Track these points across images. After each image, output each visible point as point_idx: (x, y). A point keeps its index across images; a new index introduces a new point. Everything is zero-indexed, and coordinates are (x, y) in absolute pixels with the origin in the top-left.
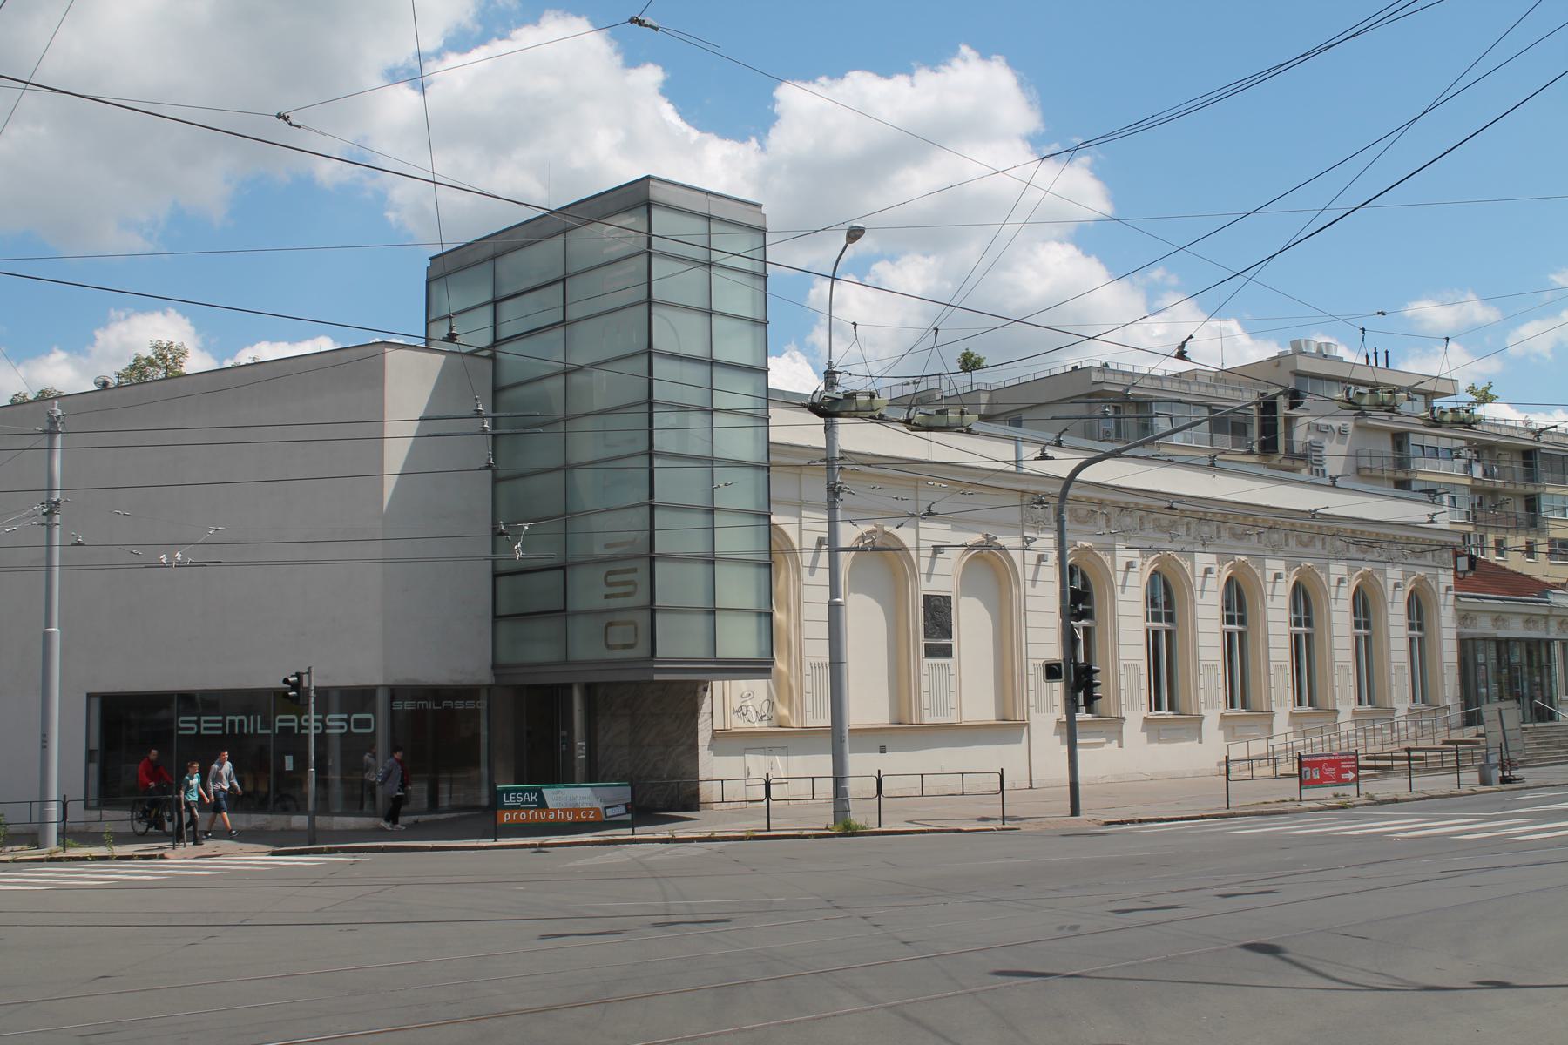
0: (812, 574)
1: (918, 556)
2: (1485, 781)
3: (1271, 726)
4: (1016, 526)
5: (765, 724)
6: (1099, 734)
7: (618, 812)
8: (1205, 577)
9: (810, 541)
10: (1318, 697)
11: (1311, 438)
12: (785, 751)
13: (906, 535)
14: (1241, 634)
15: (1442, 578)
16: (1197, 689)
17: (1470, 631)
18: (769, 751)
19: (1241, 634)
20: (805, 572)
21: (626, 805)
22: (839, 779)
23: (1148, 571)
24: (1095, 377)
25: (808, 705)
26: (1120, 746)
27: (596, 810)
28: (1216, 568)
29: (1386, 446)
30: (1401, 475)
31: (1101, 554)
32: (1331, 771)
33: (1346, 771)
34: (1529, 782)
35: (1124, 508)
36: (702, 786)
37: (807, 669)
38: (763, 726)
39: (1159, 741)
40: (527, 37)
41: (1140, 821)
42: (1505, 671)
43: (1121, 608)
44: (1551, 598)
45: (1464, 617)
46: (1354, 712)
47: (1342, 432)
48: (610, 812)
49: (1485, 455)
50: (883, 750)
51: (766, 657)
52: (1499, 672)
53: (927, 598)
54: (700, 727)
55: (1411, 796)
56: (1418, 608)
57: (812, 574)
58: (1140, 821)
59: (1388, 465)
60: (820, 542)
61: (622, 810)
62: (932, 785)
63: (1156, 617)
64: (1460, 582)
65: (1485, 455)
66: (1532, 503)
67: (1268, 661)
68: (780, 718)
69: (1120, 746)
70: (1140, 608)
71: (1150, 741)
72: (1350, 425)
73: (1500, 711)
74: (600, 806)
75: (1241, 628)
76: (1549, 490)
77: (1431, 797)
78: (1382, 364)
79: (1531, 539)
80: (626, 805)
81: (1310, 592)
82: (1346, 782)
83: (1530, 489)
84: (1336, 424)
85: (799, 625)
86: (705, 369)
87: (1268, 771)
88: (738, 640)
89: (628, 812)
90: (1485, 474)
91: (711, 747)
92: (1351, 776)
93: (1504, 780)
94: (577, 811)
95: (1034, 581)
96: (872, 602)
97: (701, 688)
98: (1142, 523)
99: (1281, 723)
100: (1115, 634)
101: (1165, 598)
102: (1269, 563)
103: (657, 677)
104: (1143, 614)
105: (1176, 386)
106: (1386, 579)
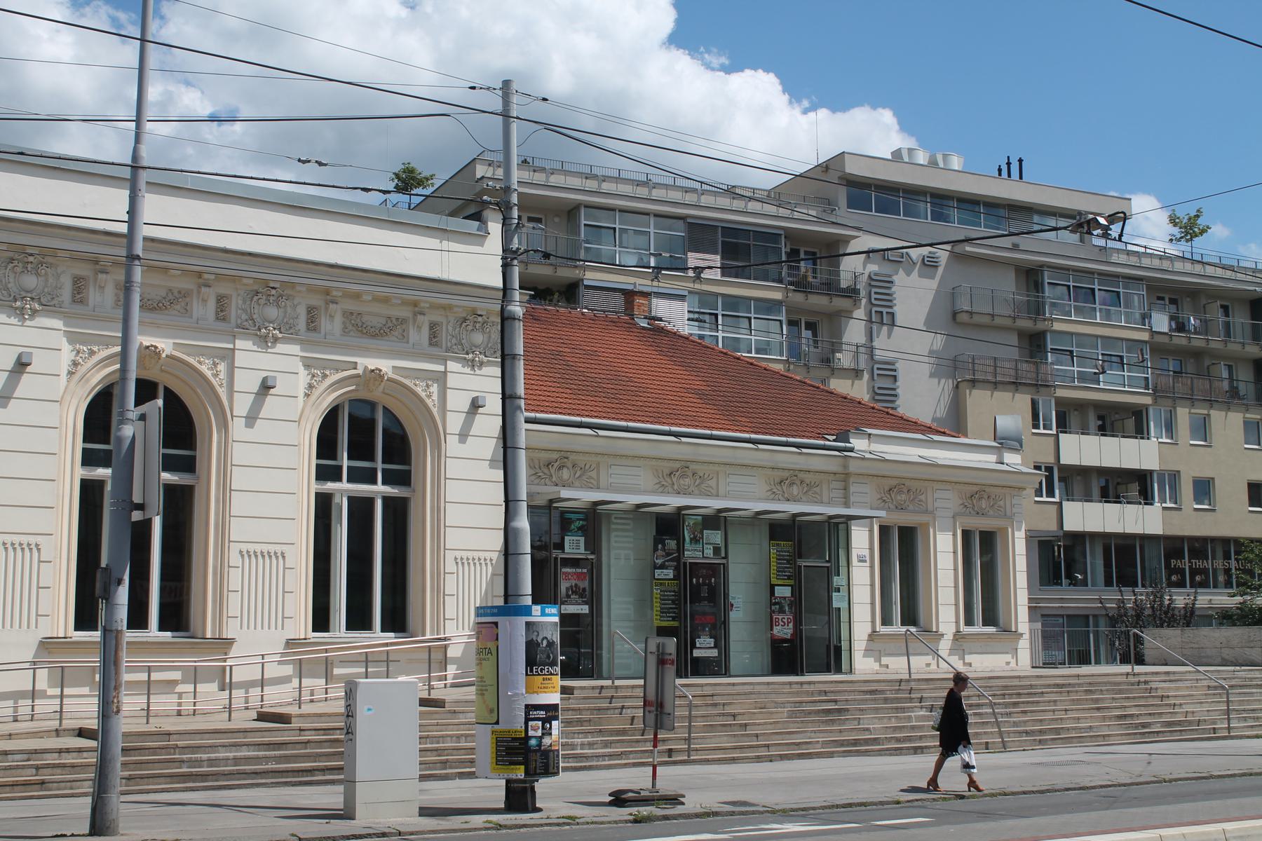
72: (943, 254)
95: (463, 436)
105: (771, 209)
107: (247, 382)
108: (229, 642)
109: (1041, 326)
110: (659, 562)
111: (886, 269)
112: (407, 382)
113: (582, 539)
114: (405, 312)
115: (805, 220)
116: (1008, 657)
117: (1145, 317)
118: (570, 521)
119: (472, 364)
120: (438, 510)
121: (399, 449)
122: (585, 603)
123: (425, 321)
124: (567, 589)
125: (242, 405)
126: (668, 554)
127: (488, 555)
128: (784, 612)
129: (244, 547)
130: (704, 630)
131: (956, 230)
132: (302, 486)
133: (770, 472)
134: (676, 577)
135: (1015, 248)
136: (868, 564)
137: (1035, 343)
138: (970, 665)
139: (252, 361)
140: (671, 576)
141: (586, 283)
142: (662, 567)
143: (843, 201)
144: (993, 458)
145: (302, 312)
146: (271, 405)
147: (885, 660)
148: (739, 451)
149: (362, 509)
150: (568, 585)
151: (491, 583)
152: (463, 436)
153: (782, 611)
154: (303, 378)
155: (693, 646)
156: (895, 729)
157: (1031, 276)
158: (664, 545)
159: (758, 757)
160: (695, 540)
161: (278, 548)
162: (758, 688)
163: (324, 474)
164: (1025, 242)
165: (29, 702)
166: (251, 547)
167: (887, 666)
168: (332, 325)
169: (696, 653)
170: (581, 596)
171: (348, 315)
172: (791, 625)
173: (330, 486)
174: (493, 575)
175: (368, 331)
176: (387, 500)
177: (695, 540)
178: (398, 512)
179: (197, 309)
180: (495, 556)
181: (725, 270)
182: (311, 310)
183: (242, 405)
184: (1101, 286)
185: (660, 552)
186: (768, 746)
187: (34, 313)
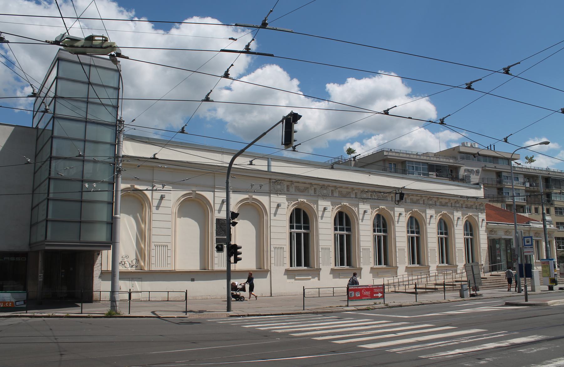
0: (322, 219)
1: (359, 214)
2: (462, 296)
3: (397, 272)
4: (149, 182)
5: (134, 268)
6: (308, 275)
7: (20, 304)
8: (430, 218)
9: (218, 201)
10: (475, 260)
11: (466, 174)
12: (140, 279)
13: (264, 199)
14: (417, 238)
15: (480, 216)
16: (359, 257)
17: (494, 236)
18: (132, 279)
19: (417, 238)
20: (154, 209)
21: (24, 301)
22: (113, 292)
23: (438, 218)
24: (385, 154)
25: (273, 261)
26: (319, 280)
27: (12, 302)
28: (461, 217)
29: (494, 176)
30: (499, 186)
31: (450, 215)
32: (368, 293)
33: (377, 293)
34: (485, 296)
35: (323, 187)
36: (94, 293)
37: (153, 247)
38: (133, 269)
39: (339, 278)
40: (259, 71)
41: (249, 315)
42: (509, 251)
43: (456, 232)
44: (531, 224)
45: (490, 231)
46: (438, 267)
47: (477, 172)
48: (17, 303)
49: (531, 180)
50: (193, 280)
51: (109, 241)
52: (507, 250)
53: (218, 220)
54: (95, 269)
55: (445, 301)
56: (470, 228)
57: (322, 219)
58: (249, 315)
59: (494, 183)
60: (223, 202)
61: (22, 303)
62: (155, 296)
63: (441, 233)
64: (489, 217)
65: (531, 180)
66: (549, 195)
67: (396, 247)
68: (141, 266)
69: (319, 280)
70: (462, 232)
71: (334, 277)
72: (480, 169)
73: (472, 266)
74: (14, 301)
75: (347, 233)
76: (554, 191)
77: (434, 303)
78: (493, 149)
79: (548, 207)
80: (24, 301)
81: (385, 217)
82: (377, 298)
83: (547, 191)
84: (475, 169)
85: (150, 229)
86: (82, 125)
87: (393, 289)
88: (102, 235)
89: (25, 304)
90: (531, 185)
91: (100, 277)
92: (380, 295)
93: (472, 295)
94: (4, 303)
95: (275, 214)
96: (193, 221)
97: (96, 254)
98: (332, 193)
99: (401, 270)
100: (317, 235)
101: (415, 226)
102: (396, 209)
103: (47, 248)
104: (437, 233)
105: (435, 159)
106: (453, 216)
107: (321, 208)
108: (320, 269)
109: (502, 187)
111: (469, 173)
114: (350, 190)
115: (451, 162)
117: (524, 183)
120: (479, 240)
121: (306, 220)
123: (354, 192)
125: (320, 214)
131: (483, 164)
132: (331, 232)
135: (495, 167)
137: (500, 190)
139: (323, 203)
143: (459, 158)
145: (285, 186)
146: (164, 203)
149: (299, 235)
154: (287, 203)
157: (499, 174)
161: (166, 244)
163: (292, 227)
164: (498, 166)
165: (446, 281)
166: (158, 244)
168: (292, 190)
171: (296, 187)
173: (292, 230)
175: (345, 196)
176: (304, 233)
178: (306, 236)
181: (437, 175)
182: (288, 186)
183: (320, 214)
184: (516, 175)
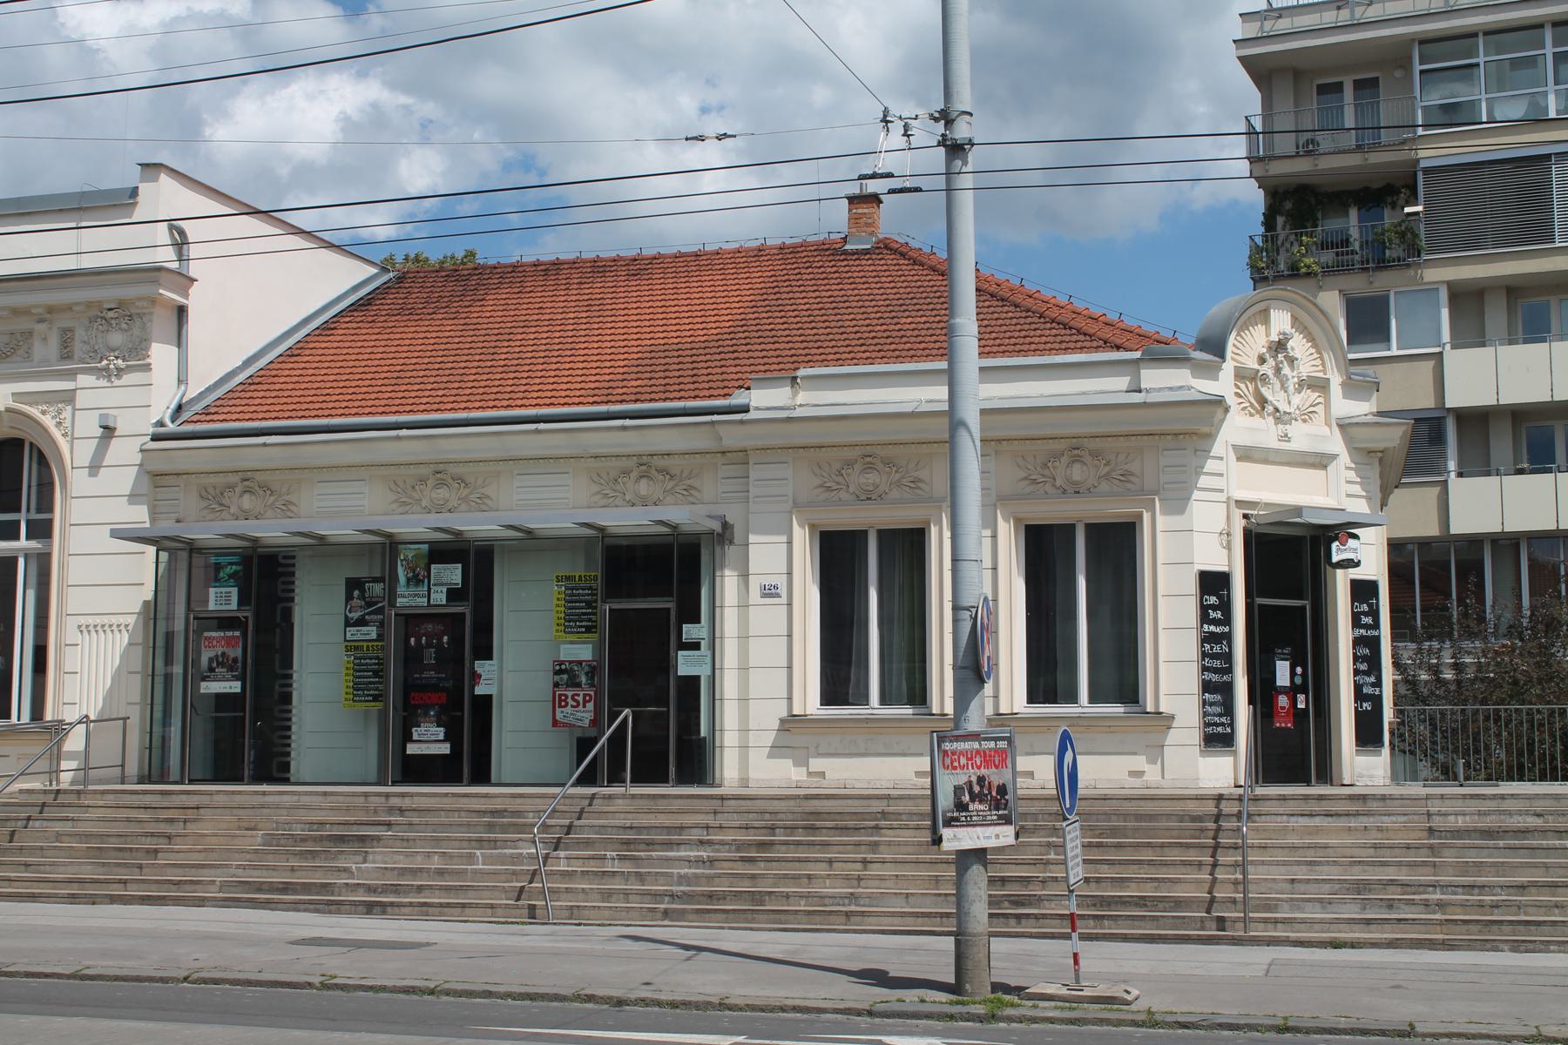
95: (94, 468)
107: (89, 426)
110: (355, 615)
112: (34, 411)
113: (234, 591)
116: (1139, 762)
118: (218, 567)
119: (106, 373)
122: (236, 678)
124: (211, 660)
126: (369, 604)
127: (122, 620)
128: (579, 685)
129: (83, 620)
130: (426, 714)
133: (592, 463)
134: (380, 637)
136: (784, 600)
138: (822, 774)
140: (374, 636)
141: (1423, 164)
142: (361, 622)
144: (1122, 382)
147: (816, 764)
148: (645, 432)
150: (211, 654)
151: (125, 656)
152: (94, 468)
153: (574, 683)
155: (408, 738)
156: (403, 872)
158: (363, 591)
159: (73, 896)
160: (414, 580)
162: (306, 800)
167: (822, 774)
169: (412, 749)
170: (231, 669)
172: (590, 706)
174: (130, 644)
177: (414, 580)
179: (38, 349)
180: (131, 620)
185: (356, 602)
186: (125, 882)
187: (120, 372)
